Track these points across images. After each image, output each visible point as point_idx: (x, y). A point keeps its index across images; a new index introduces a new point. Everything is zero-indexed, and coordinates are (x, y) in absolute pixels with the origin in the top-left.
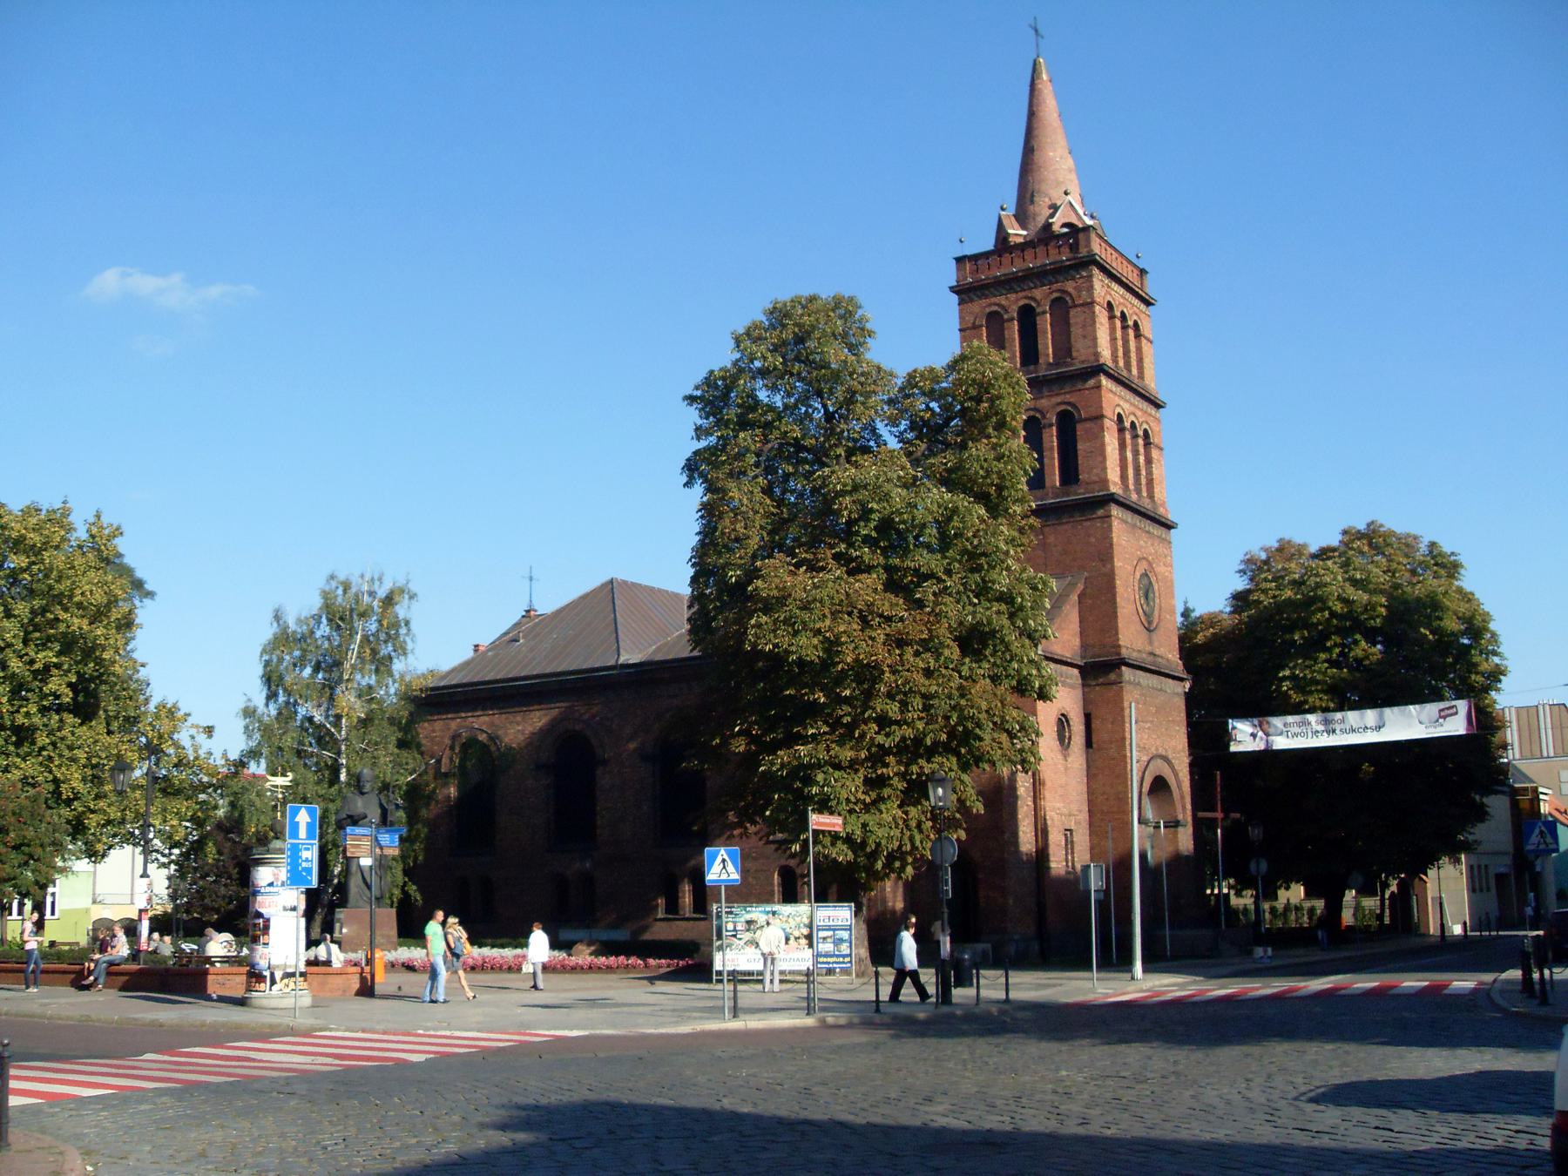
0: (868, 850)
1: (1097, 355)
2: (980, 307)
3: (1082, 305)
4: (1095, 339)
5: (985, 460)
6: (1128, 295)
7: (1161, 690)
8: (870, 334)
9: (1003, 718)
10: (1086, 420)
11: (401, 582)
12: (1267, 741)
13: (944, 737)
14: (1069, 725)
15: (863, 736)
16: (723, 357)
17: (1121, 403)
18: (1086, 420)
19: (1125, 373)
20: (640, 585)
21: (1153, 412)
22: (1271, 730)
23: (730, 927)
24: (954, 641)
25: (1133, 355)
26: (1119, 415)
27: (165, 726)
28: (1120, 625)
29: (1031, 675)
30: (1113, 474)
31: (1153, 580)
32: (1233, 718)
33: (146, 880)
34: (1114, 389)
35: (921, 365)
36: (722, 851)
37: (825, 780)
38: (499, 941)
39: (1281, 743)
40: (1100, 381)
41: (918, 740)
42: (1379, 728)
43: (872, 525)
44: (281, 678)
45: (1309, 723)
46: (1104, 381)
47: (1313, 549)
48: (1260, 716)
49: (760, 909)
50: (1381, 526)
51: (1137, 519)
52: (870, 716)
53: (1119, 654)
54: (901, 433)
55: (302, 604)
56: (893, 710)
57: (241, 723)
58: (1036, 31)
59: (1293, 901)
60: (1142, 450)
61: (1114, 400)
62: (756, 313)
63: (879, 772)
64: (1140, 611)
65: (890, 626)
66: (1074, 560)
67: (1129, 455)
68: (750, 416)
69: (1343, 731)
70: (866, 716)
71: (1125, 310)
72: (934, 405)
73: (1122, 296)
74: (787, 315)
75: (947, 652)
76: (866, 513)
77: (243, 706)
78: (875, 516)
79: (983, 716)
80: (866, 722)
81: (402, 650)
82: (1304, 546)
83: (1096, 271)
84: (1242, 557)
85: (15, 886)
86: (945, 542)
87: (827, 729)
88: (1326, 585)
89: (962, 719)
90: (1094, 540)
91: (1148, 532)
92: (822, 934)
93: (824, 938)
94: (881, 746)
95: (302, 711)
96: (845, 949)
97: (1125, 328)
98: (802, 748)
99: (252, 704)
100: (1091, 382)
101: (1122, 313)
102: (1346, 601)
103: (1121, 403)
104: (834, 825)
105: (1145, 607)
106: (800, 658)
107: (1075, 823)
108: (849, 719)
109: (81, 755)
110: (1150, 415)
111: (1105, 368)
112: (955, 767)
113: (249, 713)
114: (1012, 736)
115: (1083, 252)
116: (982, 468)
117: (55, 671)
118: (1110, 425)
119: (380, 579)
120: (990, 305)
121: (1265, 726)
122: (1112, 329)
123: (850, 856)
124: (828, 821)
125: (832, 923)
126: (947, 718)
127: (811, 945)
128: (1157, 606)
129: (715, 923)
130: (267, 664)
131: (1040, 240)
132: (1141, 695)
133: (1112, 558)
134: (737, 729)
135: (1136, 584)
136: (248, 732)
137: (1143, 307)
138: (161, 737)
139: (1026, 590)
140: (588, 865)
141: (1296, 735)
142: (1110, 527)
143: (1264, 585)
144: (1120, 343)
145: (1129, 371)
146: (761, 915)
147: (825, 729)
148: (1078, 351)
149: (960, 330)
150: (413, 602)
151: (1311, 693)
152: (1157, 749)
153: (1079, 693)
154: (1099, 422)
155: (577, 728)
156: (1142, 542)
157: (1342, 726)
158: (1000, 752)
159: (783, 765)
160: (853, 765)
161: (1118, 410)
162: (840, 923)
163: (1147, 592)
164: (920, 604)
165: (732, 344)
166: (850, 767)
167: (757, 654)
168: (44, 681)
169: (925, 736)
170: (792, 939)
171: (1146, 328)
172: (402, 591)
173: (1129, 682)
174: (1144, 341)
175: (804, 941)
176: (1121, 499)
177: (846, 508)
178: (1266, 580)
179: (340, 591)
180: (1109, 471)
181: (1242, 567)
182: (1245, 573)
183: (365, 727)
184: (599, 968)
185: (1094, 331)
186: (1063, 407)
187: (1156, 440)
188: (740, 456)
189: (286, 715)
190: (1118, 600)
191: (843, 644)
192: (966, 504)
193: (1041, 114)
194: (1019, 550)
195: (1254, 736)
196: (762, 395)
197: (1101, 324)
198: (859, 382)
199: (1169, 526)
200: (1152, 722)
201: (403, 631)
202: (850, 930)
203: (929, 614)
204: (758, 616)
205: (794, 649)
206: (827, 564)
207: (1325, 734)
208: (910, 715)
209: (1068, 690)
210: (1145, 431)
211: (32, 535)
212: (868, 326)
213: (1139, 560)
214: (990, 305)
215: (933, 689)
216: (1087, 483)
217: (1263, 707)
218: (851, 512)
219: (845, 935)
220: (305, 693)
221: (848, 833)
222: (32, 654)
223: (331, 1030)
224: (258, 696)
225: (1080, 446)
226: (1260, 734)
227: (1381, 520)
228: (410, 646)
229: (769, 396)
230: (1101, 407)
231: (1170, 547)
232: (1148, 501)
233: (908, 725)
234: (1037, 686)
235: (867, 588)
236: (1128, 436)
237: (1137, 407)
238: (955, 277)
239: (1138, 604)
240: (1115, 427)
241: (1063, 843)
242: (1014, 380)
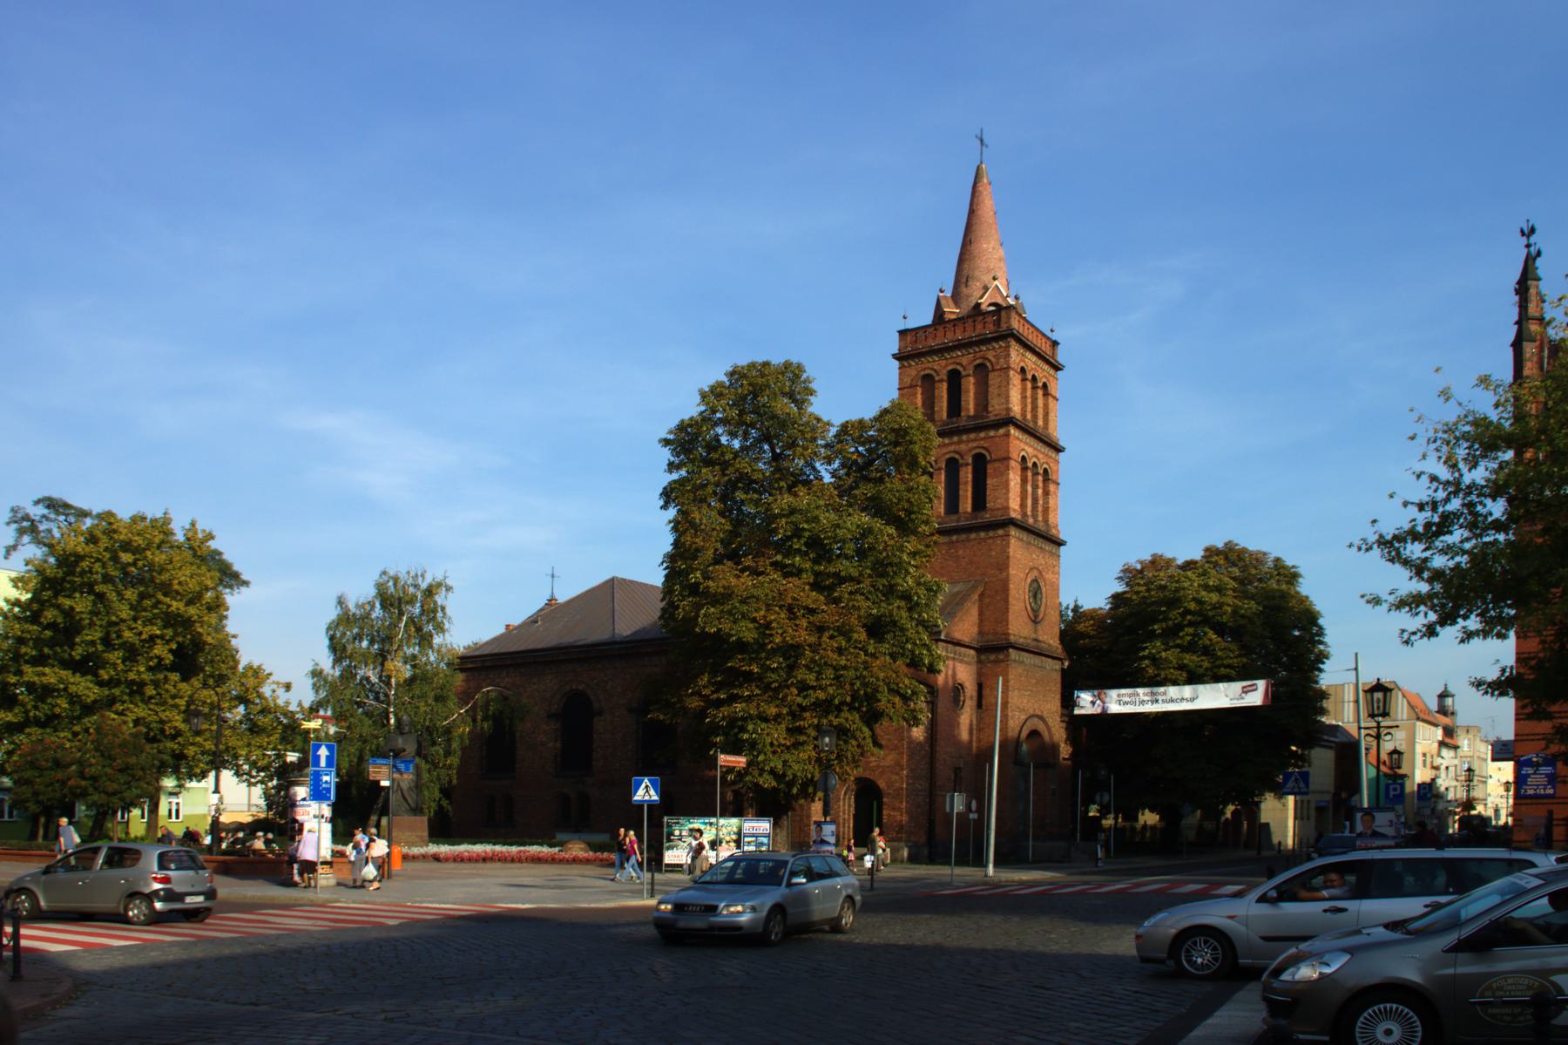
0: (787, 779)
1: (1008, 410)
2: (916, 369)
3: (1000, 369)
4: (1007, 397)
5: (897, 491)
6: (1040, 362)
8: (812, 392)
10: (995, 460)
11: (439, 578)
13: (848, 699)
14: (964, 692)
15: (785, 696)
16: (691, 408)
17: (1026, 448)
18: (995, 460)
19: (1031, 425)
20: (636, 582)
21: (1053, 455)
23: (677, 833)
27: (251, 682)
28: (1011, 618)
30: (1014, 504)
31: (1042, 584)
33: (217, 796)
36: (646, 780)
38: (509, 841)
39: (1114, 708)
40: (1009, 431)
42: (1192, 700)
44: (344, 648)
47: (1180, 562)
50: (1237, 545)
51: (1032, 538)
52: (792, 682)
55: (361, 591)
56: (811, 678)
57: (310, 681)
58: (982, 141)
60: (1041, 484)
61: (1020, 445)
62: (717, 374)
64: (1029, 608)
67: (1029, 489)
68: (714, 455)
72: (860, 449)
74: (744, 376)
75: (855, 636)
76: (797, 533)
77: (311, 669)
78: (807, 534)
80: (788, 687)
81: (440, 628)
82: (1174, 559)
83: (1013, 343)
84: (1121, 568)
85: (120, 799)
86: (862, 553)
87: (759, 692)
88: (1184, 589)
89: (865, 685)
90: (994, 553)
92: (747, 839)
95: (361, 673)
97: (1034, 388)
99: (319, 668)
100: (1002, 431)
102: (1199, 602)
103: (1026, 448)
104: (739, 762)
108: (777, 685)
109: (182, 703)
110: (1051, 457)
112: (857, 721)
113: (317, 674)
115: (1004, 327)
116: (895, 496)
117: (159, 641)
118: (1015, 465)
119: (423, 576)
120: (925, 369)
121: (1103, 696)
122: (1024, 390)
123: (774, 784)
126: (852, 685)
129: (665, 830)
130: (332, 638)
131: (969, 317)
133: (1008, 567)
135: (1027, 587)
136: (316, 688)
137: (1052, 372)
138: (247, 690)
139: (922, 591)
141: (1126, 703)
142: (1008, 543)
144: (1029, 400)
145: (1036, 423)
147: (757, 691)
149: (899, 389)
150: (450, 593)
153: (973, 668)
154: (1006, 463)
155: (580, 688)
156: (1034, 556)
157: (1164, 697)
160: (777, 718)
161: (1023, 453)
165: (698, 399)
167: (704, 634)
168: (151, 648)
169: (835, 698)
171: (1052, 389)
172: (439, 585)
173: (1015, 661)
174: (1051, 399)
175: (733, 844)
178: (1139, 584)
179: (391, 583)
180: (1011, 501)
181: (1121, 575)
183: (409, 685)
184: (568, 861)
185: (1008, 391)
186: (952, 455)
189: (348, 675)
190: (1010, 599)
193: (980, 212)
196: (724, 440)
197: (1014, 385)
198: (799, 431)
199: (1060, 543)
200: (1031, 691)
201: (440, 615)
203: (843, 607)
205: (733, 632)
209: (964, 666)
210: (1045, 470)
211: (136, 538)
212: (813, 386)
213: (1031, 569)
214: (925, 369)
215: (843, 662)
216: (992, 510)
217: (1103, 681)
218: (786, 531)
219: (765, 840)
220: (365, 658)
222: (140, 628)
223: (341, 902)
224: (326, 662)
225: (989, 481)
226: (1098, 702)
228: (447, 626)
232: (1042, 524)
235: (799, 590)
236: (1029, 474)
238: (897, 347)
240: (1019, 467)
241: (953, 777)
242: (926, 429)
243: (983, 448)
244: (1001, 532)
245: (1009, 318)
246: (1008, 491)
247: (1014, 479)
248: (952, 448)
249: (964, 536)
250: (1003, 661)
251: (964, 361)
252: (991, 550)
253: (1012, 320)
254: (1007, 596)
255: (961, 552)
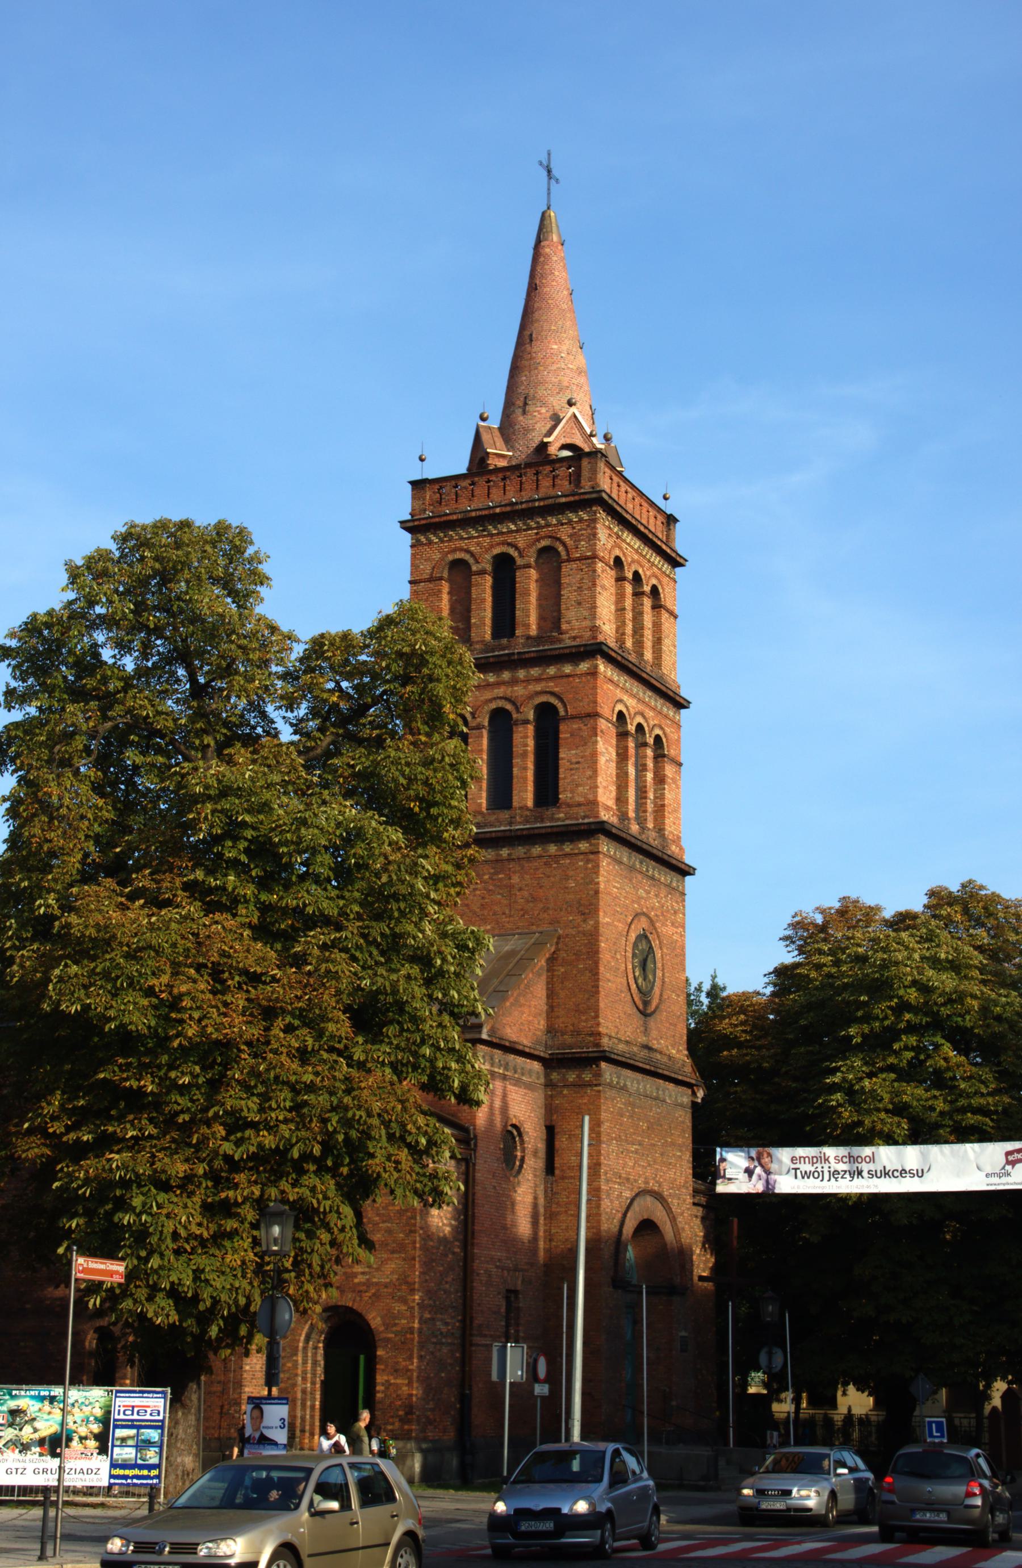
0: (202, 1307)
1: (595, 629)
3: (579, 559)
4: (593, 608)
5: (408, 764)
6: (646, 550)
7: (656, 1098)
9: (403, 1126)
10: (573, 717)
12: (767, 1182)
15: (204, 1140)
17: (625, 698)
18: (573, 717)
19: (633, 658)
21: (671, 713)
22: (774, 1167)
24: (344, 1013)
25: (648, 634)
26: (621, 714)
29: (450, 1069)
30: (606, 796)
31: (655, 944)
32: (722, 1146)
34: (616, 678)
35: (335, 627)
37: (144, 1204)
39: (786, 1185)
40: (596, 667)
41: (281, 1153)
43: (242, 845)
45: (827, 1160)
46: (602, 667)
47: (888, 914)
48: (758, 1146)
49: (32, 1393)
50: (982, 887)
51: (636, 859)
52: (216, 1114)
53: (598, 1045)
54: (301, 720)
59: (857, 1411)
60: (650, 764)
63: (223, 1195)
64: (634, 987)
65: (255, 988)
66: (545, 910)
67: (632, 770)
69: (872, 1174)
70: (211, 1114)
71: (641, 571)
73: (636, 551)
76: (233, 830)
79: (375, 1121)
82: (878, 909)
83: (601, 514)
86: (344, 874)
87: (154, 1131)
88: (897, 963)
89: (347, 1123)
91: (653, 878)
92: (120, 1433)
93: (123, 1440)
94: (228, 1159)
96: (152, 1456)
97: (638, 594)
98: (117, 1156)
100: (584, 666)
101: (636, 574)
103: (625, 698)
104: (111, 1274)
105: (640, 981)
106: (122, 1026)
107: (523, 1281)
108: (187, 1117)
110: (666, 717)
111: (604, 648)
114: (414, 1150)
115: (586, 486)
118: (606, 727)
120: (454, 550)
121: (766, 1160)
122: (620, 597)
123: (174, 1317)
124: (102, 1267)
125: (135, 1417)
126: (324, 1121)
127: (103, 1450)
128: (658, 983)
131: (528, 465)
132: (628, 1104)
133: (596, 910)
134: (26, 1125)
135: (629, 949)
137: (666, 568)
139: (449, 949)
140: (770, 1308)
141: (806, 1175)
142: (597, 866)
143: (816, 959)
144: (629, 615)
146: (32, 1402)
147: (151, 1130)
148: (568, 622)
149: (410, 582)
151: (869, 1112)
152: (646, 1182)
153: (538, 1097)
157: (872, 1166)
158: (396, 1175)
159: (87, 1181)
161: (619, 707)
162: (148, 1417)
163: (645, 959)
164: (299, 961)
165: (64, 578)
166: (182, 1187)
169: (292, 1146)
170: (76, 1439)
171: (667, 597)
173: (610, 1085)
174: (665, 615)
175: (92, 1444)
176: (614, 831)
177: (206, 818)
178: (820, 952)
180: (600, 791)
182: (793, 942)
185: (594, 597)
186: (501, 704)
187: (672, 753)
188: (68, 737)
190: (602, 969)
191: (185, 1009)
192: (374, 824)
194: (452, 891)
195: (749, 1172)
196: (107, 654)
197: (603, 587)
198: (240, 647)
202: (162, 1428)
203: (309, 974)
204: (66, 966)
205: (112, 1013)
206: (175, 896)
207: (847, 1175)
208: (273, 1115)
212: (265, 568)
214: (454, 550)
215: (308, 1078)
216: (569, 806)
218: (212, 826)
219: (154, 1435)
221: (172, 1283)
226: (758, 1170)
227: (980, 881)
229: (114, 656)
230: (595, 702)
231: (684, 900)
232: (652, 834)
233: (269, 1129)
234: (456, 1084)
237: (648, 705)
239: (631, 976)
241: (503, 1310)
243: (553, 694)
244: (583, 846)
245: (594, 471)
246: (595, 772)
247: (606, 750)
248: (500, 691)
249: (520, 851)
250: (590, 1085)
251: (521, 540)
252: (567, 878)
253: (600, 475)
254: (596, 963)
255: (515, 879)
